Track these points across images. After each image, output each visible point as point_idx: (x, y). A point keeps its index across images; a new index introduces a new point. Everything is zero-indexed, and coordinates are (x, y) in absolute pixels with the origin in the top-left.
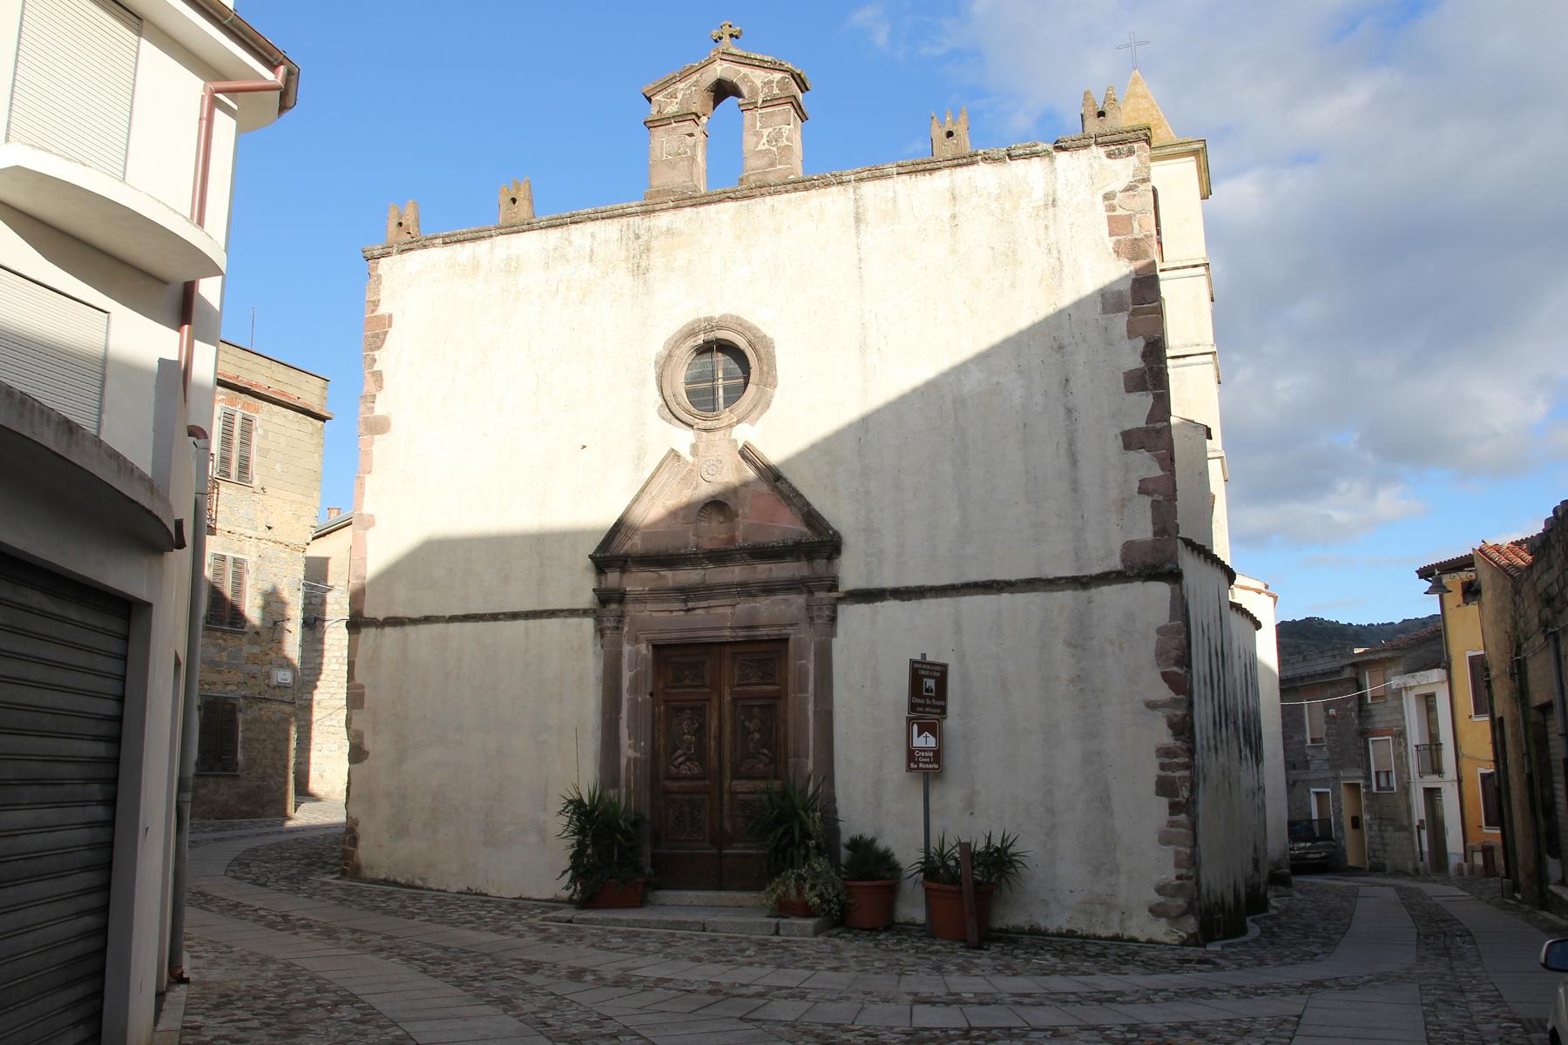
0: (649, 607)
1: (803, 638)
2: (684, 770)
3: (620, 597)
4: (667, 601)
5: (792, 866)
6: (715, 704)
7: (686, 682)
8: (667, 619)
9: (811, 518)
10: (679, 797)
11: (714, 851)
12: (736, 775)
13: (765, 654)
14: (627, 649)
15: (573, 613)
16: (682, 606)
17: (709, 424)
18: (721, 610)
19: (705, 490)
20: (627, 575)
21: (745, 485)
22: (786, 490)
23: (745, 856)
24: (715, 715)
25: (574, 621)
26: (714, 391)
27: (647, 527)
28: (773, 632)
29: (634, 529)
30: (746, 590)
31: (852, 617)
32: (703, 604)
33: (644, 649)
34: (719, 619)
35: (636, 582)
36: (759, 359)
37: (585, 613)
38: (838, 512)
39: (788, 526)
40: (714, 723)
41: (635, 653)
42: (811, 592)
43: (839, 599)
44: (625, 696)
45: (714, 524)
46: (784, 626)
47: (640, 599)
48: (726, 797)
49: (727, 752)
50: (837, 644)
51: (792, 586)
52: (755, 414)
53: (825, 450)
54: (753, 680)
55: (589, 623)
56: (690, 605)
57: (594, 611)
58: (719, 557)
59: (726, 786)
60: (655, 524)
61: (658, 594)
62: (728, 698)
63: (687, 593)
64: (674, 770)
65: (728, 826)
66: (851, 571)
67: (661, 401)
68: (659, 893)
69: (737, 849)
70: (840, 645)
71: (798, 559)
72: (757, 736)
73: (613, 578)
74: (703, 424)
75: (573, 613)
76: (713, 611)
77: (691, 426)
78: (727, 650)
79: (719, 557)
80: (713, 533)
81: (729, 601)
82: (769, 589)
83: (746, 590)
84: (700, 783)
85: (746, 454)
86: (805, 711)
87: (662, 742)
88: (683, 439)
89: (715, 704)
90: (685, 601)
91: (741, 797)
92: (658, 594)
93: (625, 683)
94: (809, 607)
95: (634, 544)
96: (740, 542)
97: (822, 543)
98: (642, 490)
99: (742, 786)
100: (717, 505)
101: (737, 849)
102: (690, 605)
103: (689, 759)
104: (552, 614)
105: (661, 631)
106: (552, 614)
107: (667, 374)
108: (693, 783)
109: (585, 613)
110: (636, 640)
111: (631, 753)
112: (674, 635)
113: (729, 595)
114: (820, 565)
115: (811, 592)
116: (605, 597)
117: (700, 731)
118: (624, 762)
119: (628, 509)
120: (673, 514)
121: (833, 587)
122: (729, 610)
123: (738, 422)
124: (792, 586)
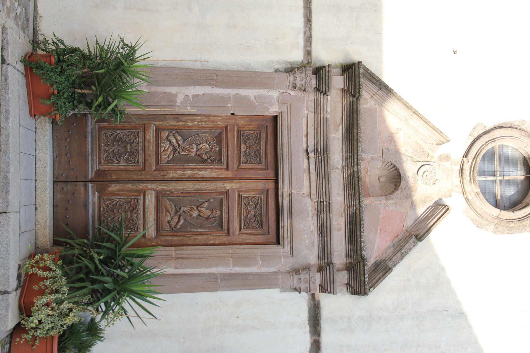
0: (312, 116)
1: (279, 259)
2: (165, 145)
3: (322, 89)
4: (316, 134)
5: (72, 290)
6: (224, 174)
7: (243, 148)
8: (297, 138)
9: (383, 269)
10: (140, 140)
11: (91, 175)
12: (160, 196)
13: (269, 223)
14: (275, 94)
15: (308, 40)
16: (311, 148)
17: (467, 172)
18: (306, 183)
19: (409, 169)
20: (340, 93)
21: (413, 206)
22: (407, 246)
23: (86, 205)
24: (214, 175)
25: (301, 41)
26: (493, 173)
27: (381, 112)
28: (285, 232)
29: (381, 103)
30: (323, 208)
31: (299, 304)
32: (312, 167)
33: (273, 110)
34: (299, 183)
35: (335, 103)
36: (520, 219)
37: (308, 53)
38: (386, 293)
39: (375, 247)
40: (206, 174)
41: (269, 101)
42: (320, 269)
43: (313, 295)
44: (233, 92)
45: (378, 172)
46: (292, 241)
47: (318, 108)
48: (141, 186)
49: (180, 186)
50: (274, 293)
51: (325, 250)
52: (473, 215)
53: (439, 282)
54: (244, 211)
55: (297, 56)
56: (312, 155)
57: (309, 63)
58: (353, 185)
59: (150, 185)
60: (384, 121)
61: (322, 125)
62: (229, 185)
63: (322, 153)
64: (164, 135)
65: (114, 187)
66: (337, 305)
67: (488, 128)
68: (48, 128)
69: (93, 198)
70: (273, 294)
71: (348, 256)
72: (195, 214)
73: (338, 82)
74: (467, 167)
75: (308, 40)
76: (306, 176)
77: (466, 155)
78: (271, 185)
79: (353, 185)
80: (372, 171)
81: (314, 192)
82: (324, 230)
83: (323, 208)
84: (153, 160)
85: (439, 208)
86: (217, 265)
87: (190, 124)
88: (456, 149)
89: (224, 174)
90: (316, 151)
91: (141, 199)
92: (322, 125)
93: (244, 92)
94: (307, 268)
95: (367, 101)
96: (365, 201)
97: (362, 276)
98: (415, 112)
99: (151, 200)
100: (396, 179)
101: (93, 198)
102: (312, 155)
103: (175, 150)
104: (308, 20)
105: (289, 127)
106: (308, 20)
107: (514, 133)
108: (153, 153)
109: (308, 53)
110: (281, 102)
111: (180, 99)
112: (285, 140)
113: (319, 194)
114: (342, 277)
115: (320, 269)
116: (320, 72)
117: (201, 160)
118: (173, 90)
119: (400, 99)
120: (391, 139)
121: (323, 289)
122: (306, 191)
123: (467, 199)
124: (325, 250)
